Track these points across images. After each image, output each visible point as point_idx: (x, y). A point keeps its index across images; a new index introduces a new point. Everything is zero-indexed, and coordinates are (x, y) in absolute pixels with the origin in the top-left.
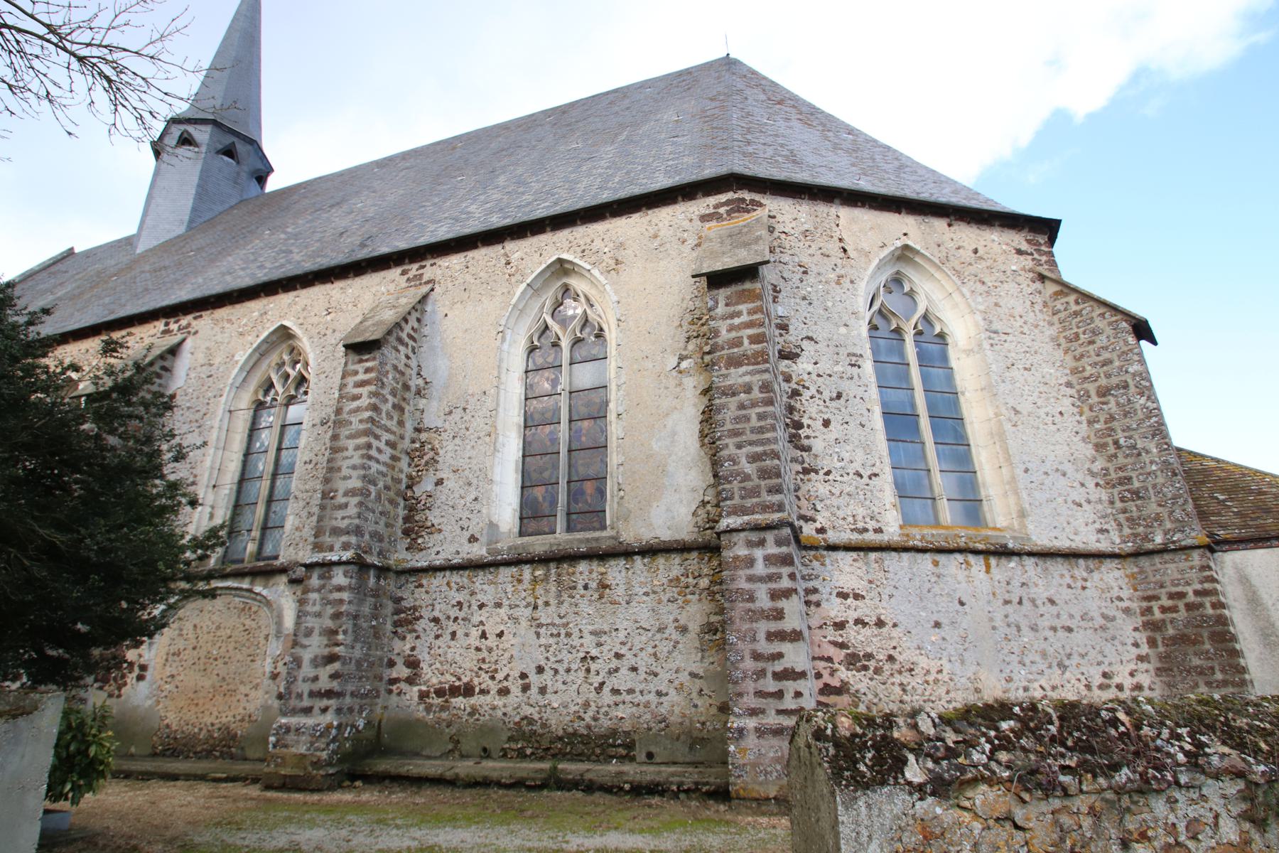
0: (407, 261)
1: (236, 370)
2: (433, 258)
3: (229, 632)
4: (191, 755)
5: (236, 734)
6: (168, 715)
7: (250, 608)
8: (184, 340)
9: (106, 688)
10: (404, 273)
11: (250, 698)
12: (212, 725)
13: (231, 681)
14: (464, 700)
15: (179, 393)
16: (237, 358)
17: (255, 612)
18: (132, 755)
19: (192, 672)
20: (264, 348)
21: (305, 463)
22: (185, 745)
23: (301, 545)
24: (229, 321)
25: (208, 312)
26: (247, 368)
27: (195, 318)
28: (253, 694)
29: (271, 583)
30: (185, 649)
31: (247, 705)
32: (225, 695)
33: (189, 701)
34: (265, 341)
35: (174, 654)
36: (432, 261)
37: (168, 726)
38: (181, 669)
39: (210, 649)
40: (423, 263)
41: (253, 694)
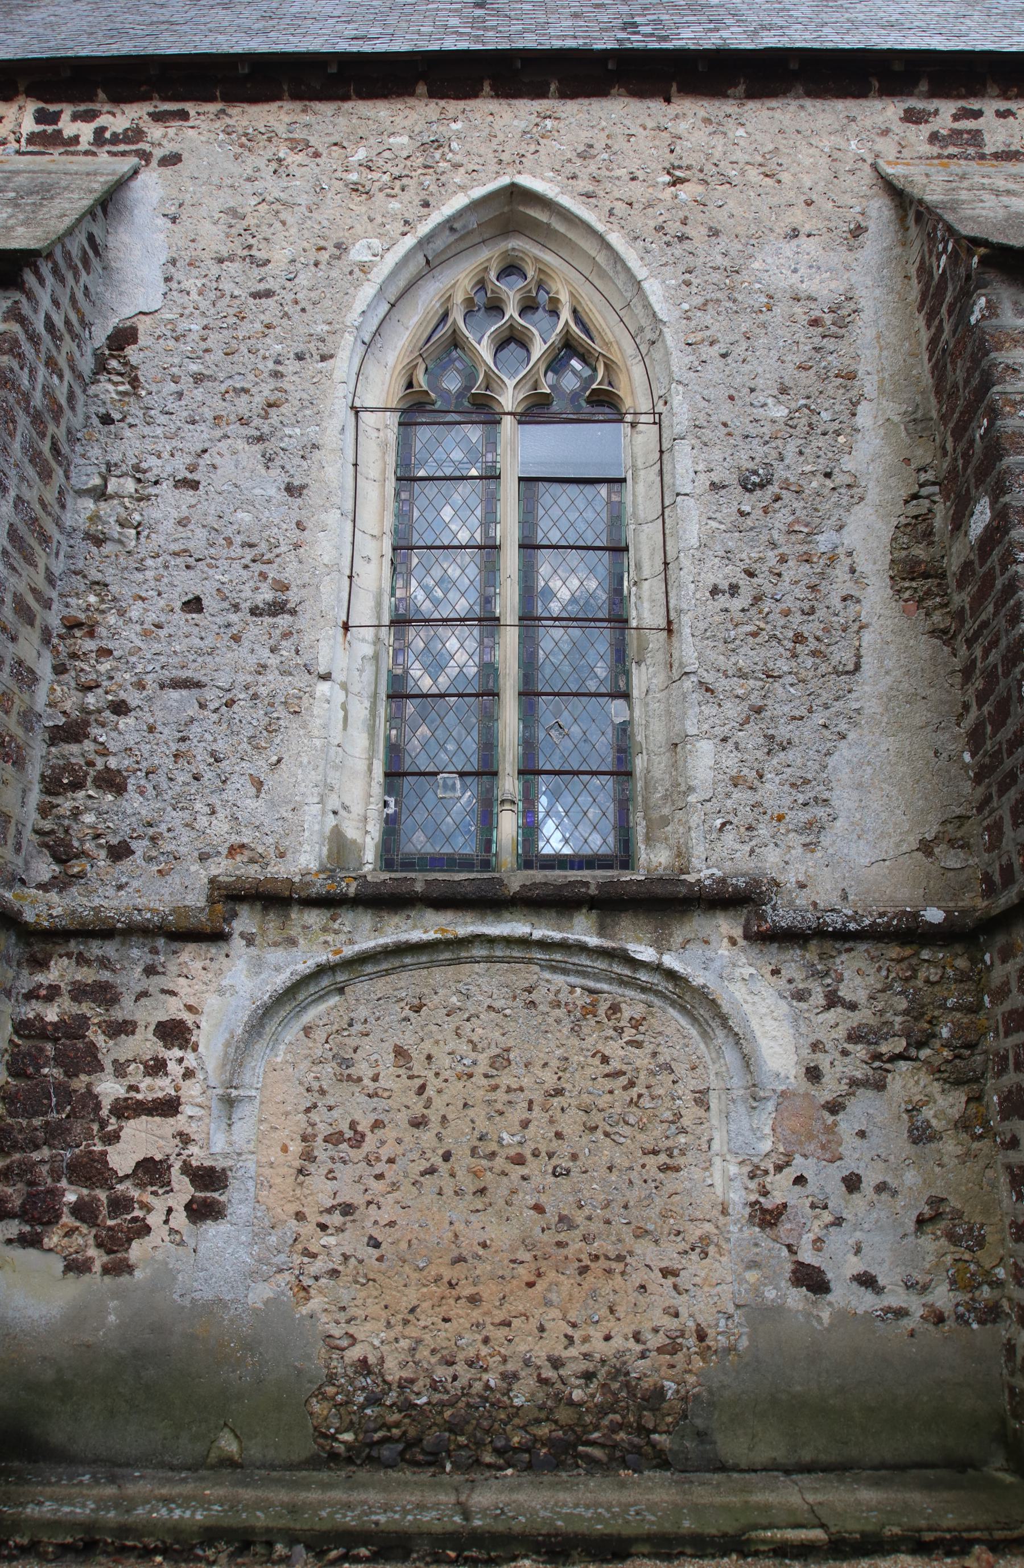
0: (924, 87)
1: (368, 291)
2: (1005, 96)
3: (549, 1079)
4: (488, 1458)
5: (659, 1392)
6: (359, 1331)
7: (615, 1009)
8: (136, 172)
9: (53, 1240)
10: (912, 117)
11: (684, 1280)
12: (556, 1363)
13: (595, 1227)
14: (674, 356)
15: (144, 325)
16: (358, 253)
17: (636, 1024)
18: (229, 1463)
19: (429, 1196)
20: (439, 244)
21: (715, 591)
22: (453, 1428)
23: (764, 831)
24: (297, 145)
25: (212, 108)
26: (392, 294)
27: (158, 117)
28: (694, 1268)
29: (678, 939)
30: (377, 1125)
31: (680, 1302)
32: (583, 1270)
33: (442, 1289)
34: (449, 225)
35: (334, 1139)
36: (1003, 105)
37: (363, 1366)
38: (377, 1186)
39: (483, 1125)
40: (975, 105)
41: (694, 1268)
